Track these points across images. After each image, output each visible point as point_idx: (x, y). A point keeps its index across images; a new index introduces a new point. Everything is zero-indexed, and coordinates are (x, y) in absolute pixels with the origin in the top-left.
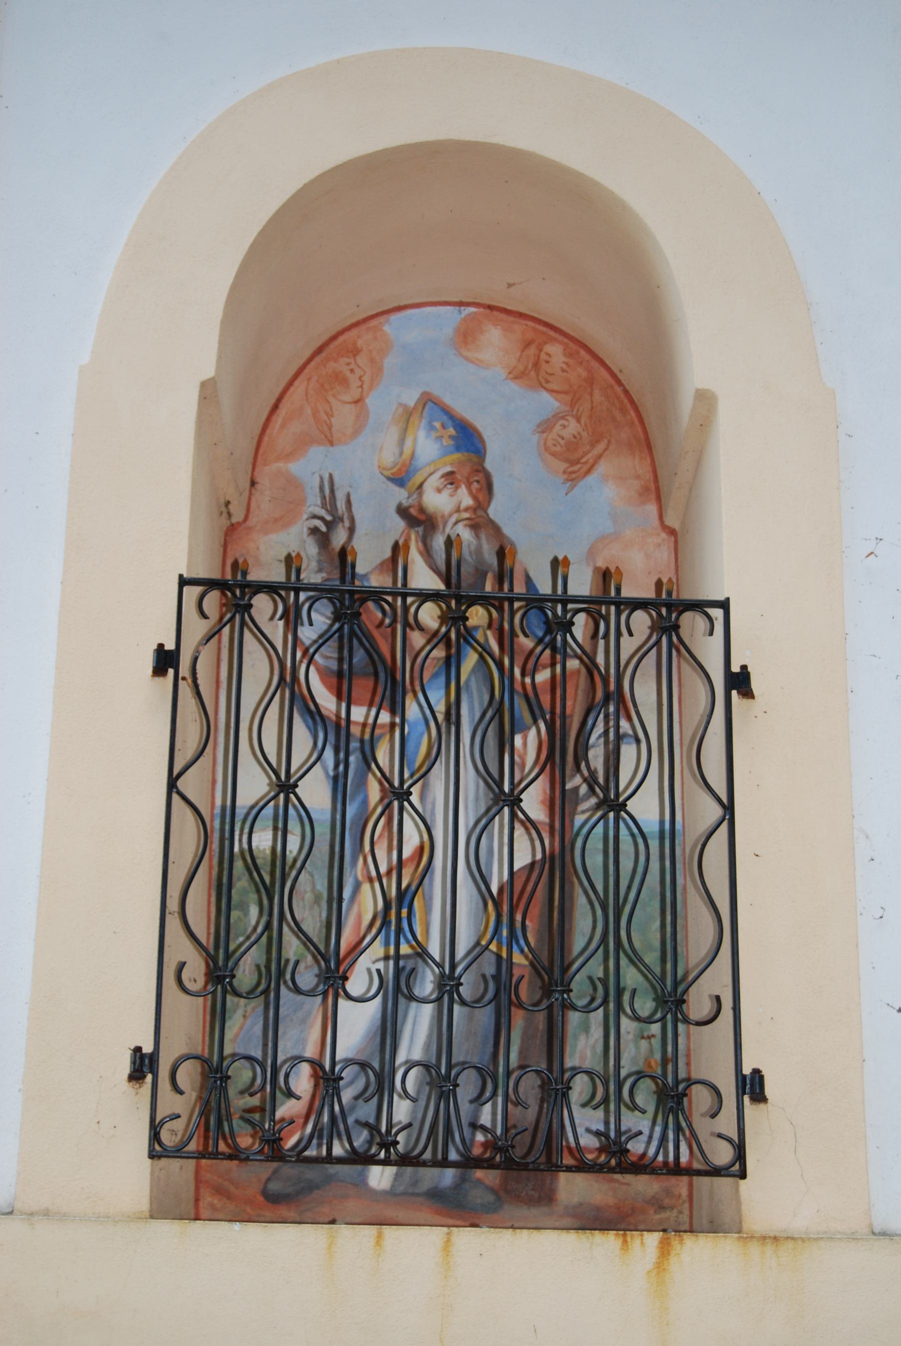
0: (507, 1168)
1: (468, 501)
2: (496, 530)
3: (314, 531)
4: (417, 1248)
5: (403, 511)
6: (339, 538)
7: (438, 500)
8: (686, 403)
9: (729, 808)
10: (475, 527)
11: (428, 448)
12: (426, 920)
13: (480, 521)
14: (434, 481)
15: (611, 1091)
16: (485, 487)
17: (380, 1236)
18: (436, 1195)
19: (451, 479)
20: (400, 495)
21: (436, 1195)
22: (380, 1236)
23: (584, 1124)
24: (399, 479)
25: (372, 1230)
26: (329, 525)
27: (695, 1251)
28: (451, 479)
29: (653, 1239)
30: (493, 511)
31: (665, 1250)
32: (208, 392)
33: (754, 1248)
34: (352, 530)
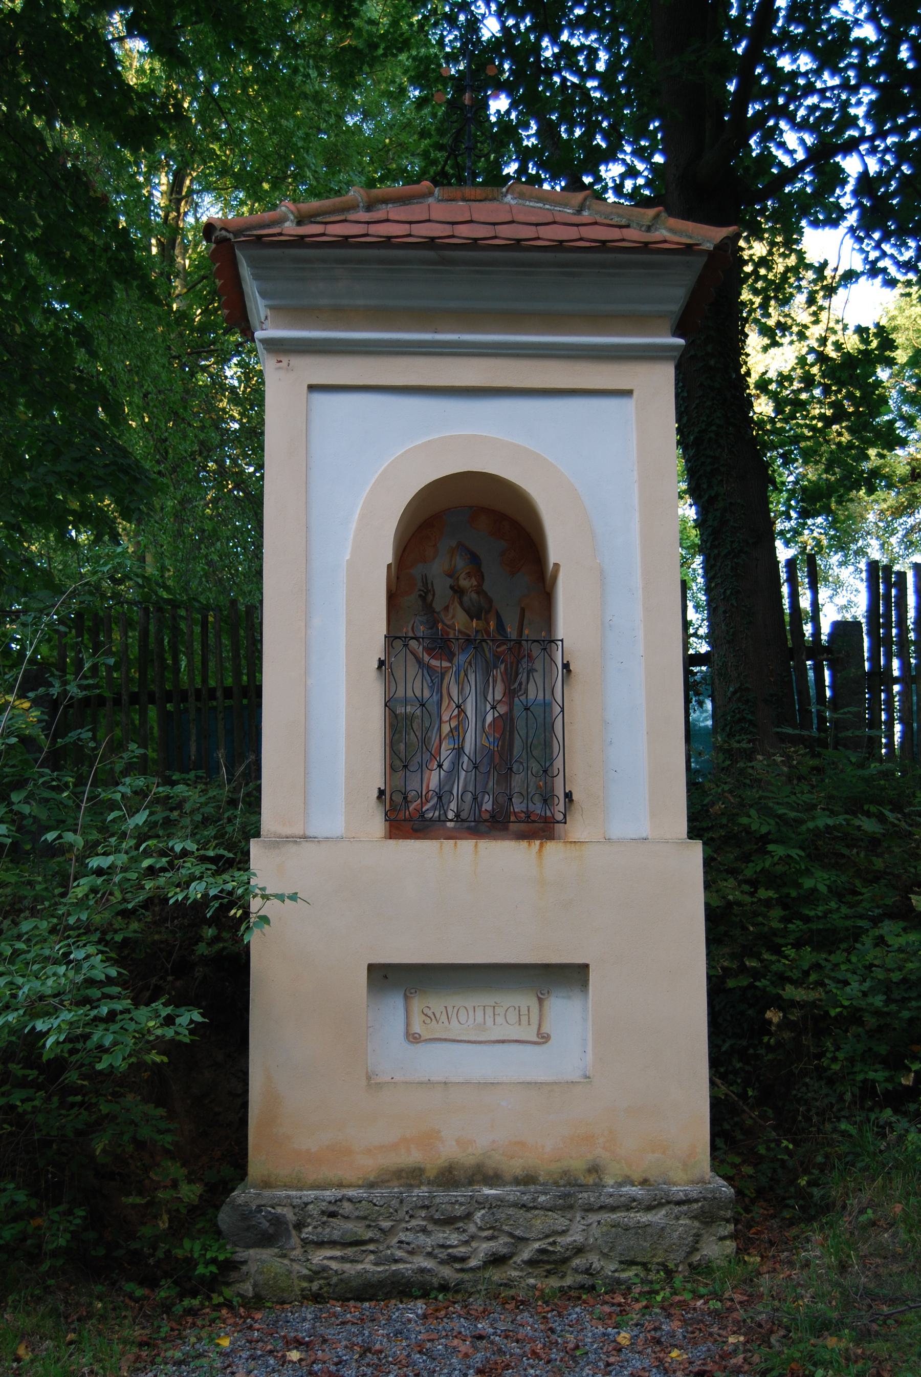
0: (493, 821)
1: (475, 583)
2: (485, 594)
3: (420, 596)
4: (466, 846)
5: (452, 587)
6: (430, 597)
7: (464, 583)
8: (551, 565)
9: (563, 711)
10: (478, 593)
11: (460, 563)
12: (618, 1207)
13: (480, 591)
14: (463, 576)
15: (526, 796)
16: (481, 578)
17: (476, 845)
18: (469, 828)
19: (469, 575)
20: (450, 581)
21: (469, 828)
22: (476, 845)
23: (518, 806)
24: (450, 575)
25: (452, 842)
26: (426, 593)
27: (551, 847)
28: (469, 575)
29: (538, 842)
30: (486, 587)
31: (541, 845)
32: (389, 566)
33: (568, 845)
34: (434, 595)
